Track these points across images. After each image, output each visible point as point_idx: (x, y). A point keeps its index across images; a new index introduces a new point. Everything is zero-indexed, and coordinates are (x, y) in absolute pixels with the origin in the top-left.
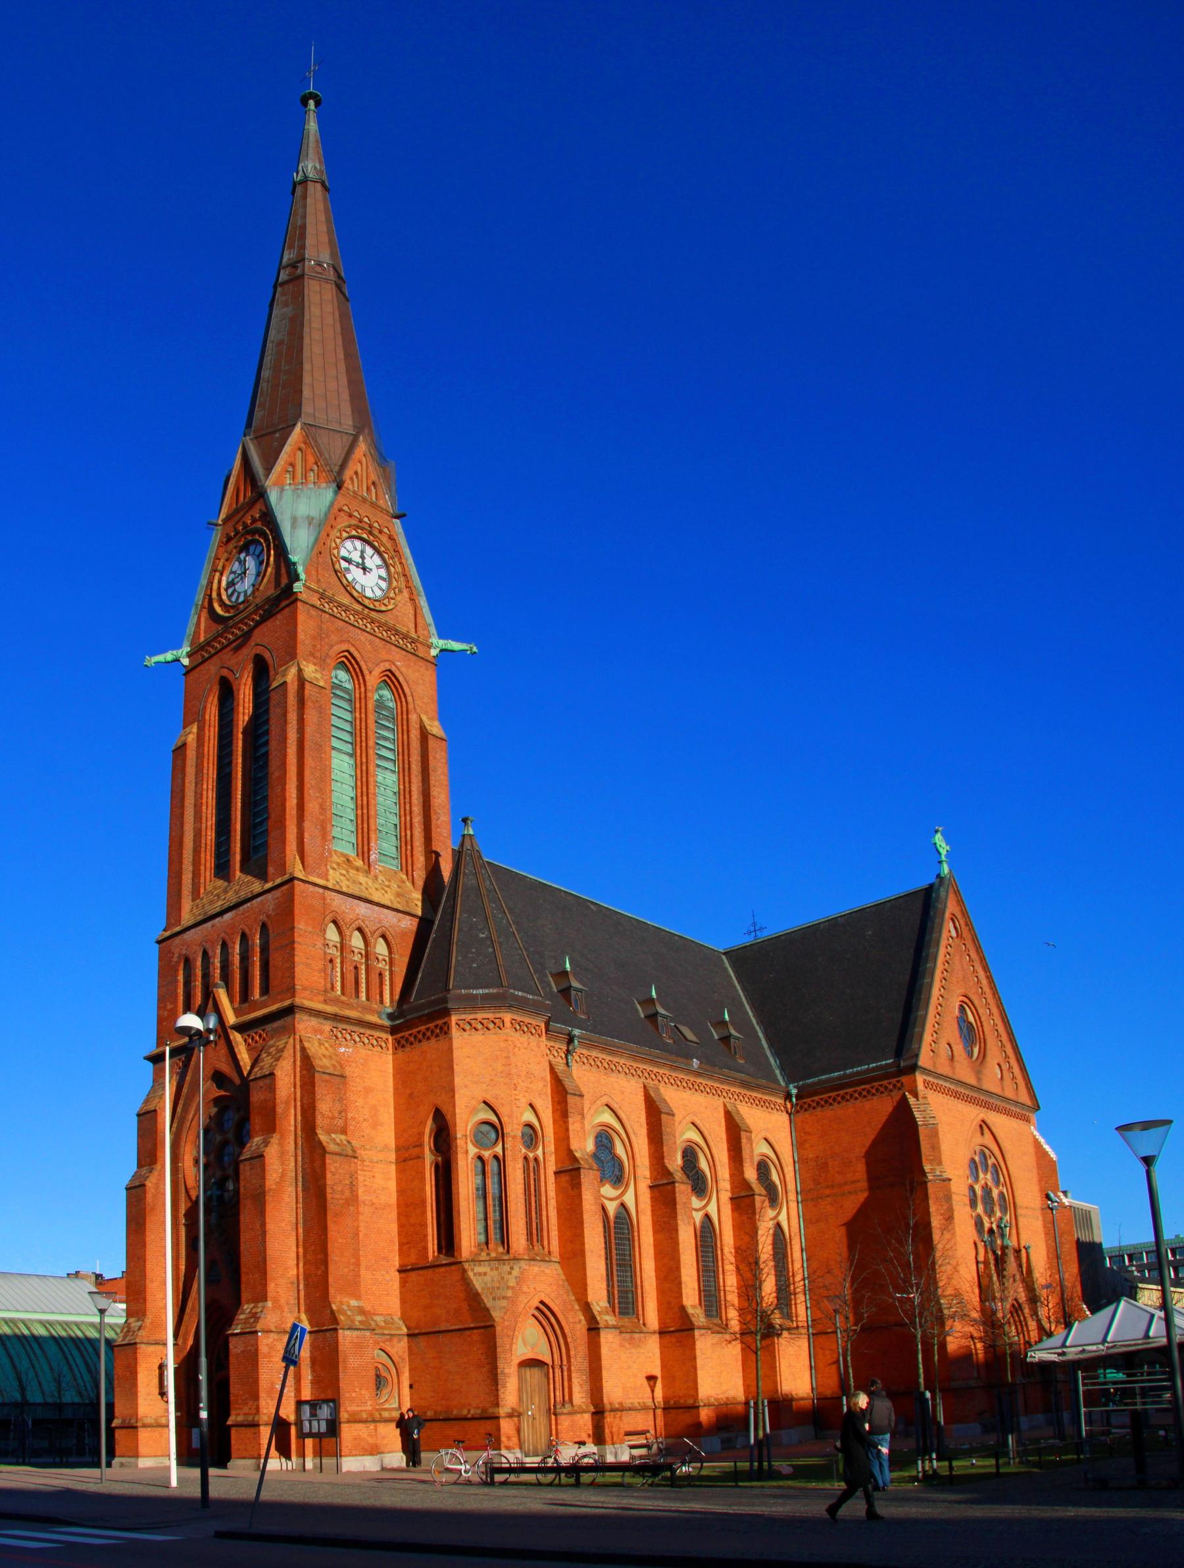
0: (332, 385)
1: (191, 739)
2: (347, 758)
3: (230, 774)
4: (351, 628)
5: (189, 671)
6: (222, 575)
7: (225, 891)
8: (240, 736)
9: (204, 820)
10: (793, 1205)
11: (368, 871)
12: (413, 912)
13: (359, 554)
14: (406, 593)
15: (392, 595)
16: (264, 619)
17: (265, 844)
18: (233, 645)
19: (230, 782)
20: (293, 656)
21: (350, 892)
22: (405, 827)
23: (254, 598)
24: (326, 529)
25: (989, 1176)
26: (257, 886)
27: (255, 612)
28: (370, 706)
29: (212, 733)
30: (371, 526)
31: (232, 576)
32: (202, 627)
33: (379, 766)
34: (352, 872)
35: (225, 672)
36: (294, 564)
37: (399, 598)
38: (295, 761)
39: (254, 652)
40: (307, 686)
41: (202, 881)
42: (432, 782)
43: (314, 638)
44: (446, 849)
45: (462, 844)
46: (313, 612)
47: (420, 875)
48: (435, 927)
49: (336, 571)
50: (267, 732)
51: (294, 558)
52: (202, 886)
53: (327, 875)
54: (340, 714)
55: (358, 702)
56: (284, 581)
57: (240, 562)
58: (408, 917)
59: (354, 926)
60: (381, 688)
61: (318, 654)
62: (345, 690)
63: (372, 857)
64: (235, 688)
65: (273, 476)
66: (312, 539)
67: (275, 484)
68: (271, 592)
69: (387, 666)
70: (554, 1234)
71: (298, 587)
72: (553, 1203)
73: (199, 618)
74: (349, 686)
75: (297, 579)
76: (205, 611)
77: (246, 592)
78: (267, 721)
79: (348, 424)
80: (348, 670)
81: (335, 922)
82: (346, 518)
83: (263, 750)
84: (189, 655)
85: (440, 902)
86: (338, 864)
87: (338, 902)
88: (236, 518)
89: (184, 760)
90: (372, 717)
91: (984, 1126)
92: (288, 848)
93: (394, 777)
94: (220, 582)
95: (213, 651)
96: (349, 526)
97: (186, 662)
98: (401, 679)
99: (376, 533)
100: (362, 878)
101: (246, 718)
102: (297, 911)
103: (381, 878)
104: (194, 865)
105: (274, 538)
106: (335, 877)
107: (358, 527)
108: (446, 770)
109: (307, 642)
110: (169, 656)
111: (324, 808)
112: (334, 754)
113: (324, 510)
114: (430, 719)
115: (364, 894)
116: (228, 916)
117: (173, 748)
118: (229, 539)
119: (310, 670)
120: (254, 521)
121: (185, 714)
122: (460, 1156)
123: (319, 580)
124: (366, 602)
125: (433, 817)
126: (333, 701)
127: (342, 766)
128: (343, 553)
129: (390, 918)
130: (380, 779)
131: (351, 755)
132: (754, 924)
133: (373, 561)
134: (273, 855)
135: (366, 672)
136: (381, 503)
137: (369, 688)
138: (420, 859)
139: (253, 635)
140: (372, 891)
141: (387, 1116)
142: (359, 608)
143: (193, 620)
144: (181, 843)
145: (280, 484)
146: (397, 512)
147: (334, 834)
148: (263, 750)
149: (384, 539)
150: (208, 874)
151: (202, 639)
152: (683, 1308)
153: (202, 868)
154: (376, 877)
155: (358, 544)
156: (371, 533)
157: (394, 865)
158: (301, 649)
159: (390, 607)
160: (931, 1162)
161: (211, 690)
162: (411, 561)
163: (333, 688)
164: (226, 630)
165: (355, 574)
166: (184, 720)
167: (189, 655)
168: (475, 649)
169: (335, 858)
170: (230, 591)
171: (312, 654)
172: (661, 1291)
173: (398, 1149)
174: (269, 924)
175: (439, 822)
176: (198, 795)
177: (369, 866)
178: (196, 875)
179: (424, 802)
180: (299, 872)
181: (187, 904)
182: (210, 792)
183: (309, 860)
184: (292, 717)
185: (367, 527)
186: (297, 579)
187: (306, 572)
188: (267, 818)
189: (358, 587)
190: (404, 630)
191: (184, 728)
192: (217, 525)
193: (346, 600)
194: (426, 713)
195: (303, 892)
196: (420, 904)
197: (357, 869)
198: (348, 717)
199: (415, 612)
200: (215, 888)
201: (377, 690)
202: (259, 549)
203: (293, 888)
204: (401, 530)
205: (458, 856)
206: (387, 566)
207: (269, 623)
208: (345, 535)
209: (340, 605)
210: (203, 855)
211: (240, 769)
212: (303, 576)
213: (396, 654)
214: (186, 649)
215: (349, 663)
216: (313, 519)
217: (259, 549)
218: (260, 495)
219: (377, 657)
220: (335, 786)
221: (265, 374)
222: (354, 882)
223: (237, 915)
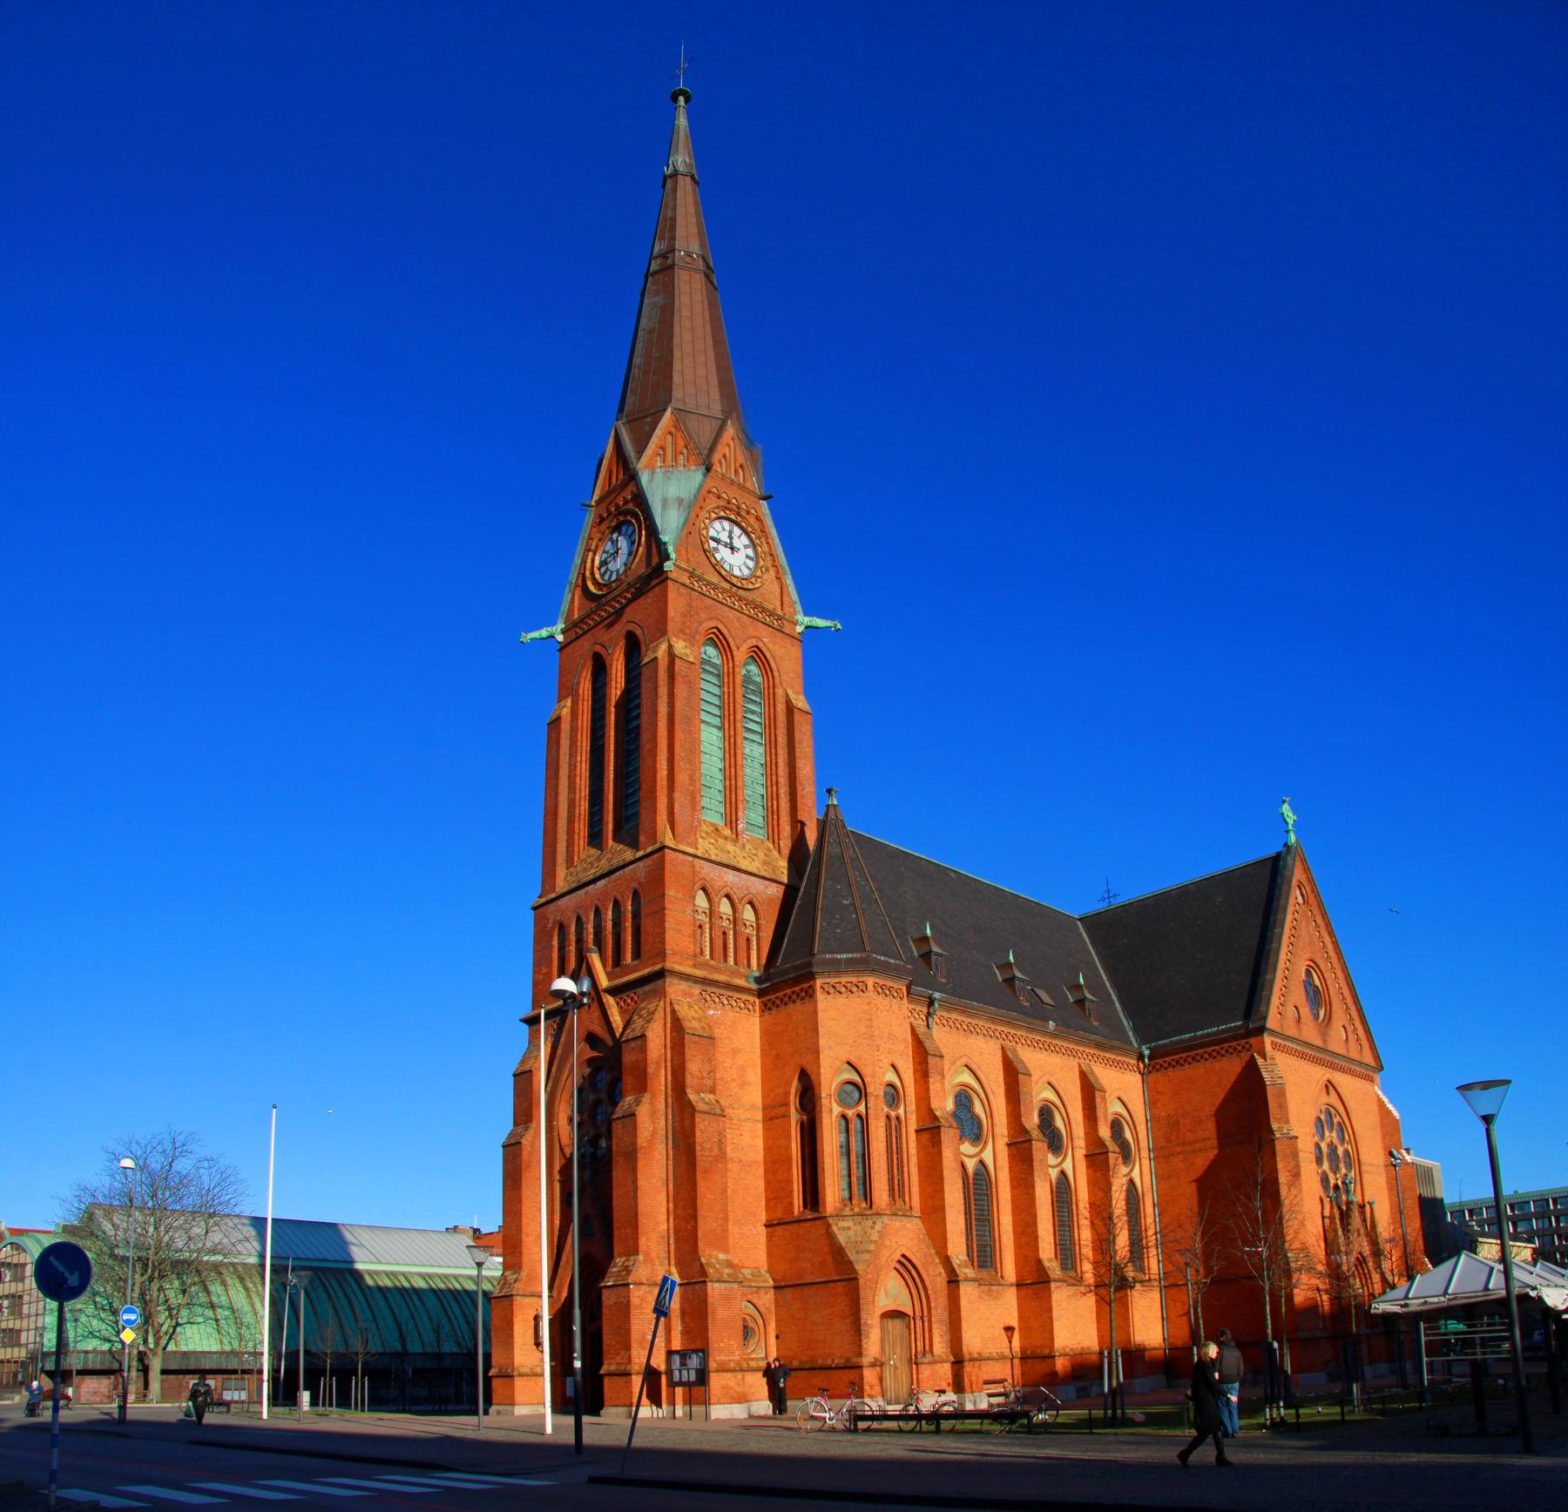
0: (701, 371)
1: (566, 712)
2: (715, 731)
5: (563, 647)
7: (599, 860)
10: (1146, 1162)
11: (736, 840)
14: (772, 572)
16: (635, 597)
17: (637, 815)
20: (664, 633)
22: (771, 798)
24: (695, 509)
25: (1334, 1134)
26: (629, 855)
27: (627, 591)
28: (738, 681)
34: (721, 841)
35: (598, 648)
40: (677, 661)
44: (811, 818)
45: (827, 815)
46: (683, 590)
47: (786, 844)
51: (664, 538)
54: (709, 689)
55: (726, 677)
56: (655, 560)
62: (714, 666)
66: (682, 520)
67: (647, 467)
68: (643, 571)
70: (915, 1190)
71: (668, 566)
72: (914, 1160)
74: (717, 661)
75: (668, 558)
78: (639, 696)
79: (717, 408)
80: (716, 646)
81: (704, 889)
83: (635, 723)
84: (564, 632)
87: (706, 870)
89: (559, 733)
90: (739, 692)
91: (1329, 1086)
93: (762, 750)
97: (560, 638)
100: (730, 847)
103: (748, 846)
106: (704, 846)
110: (544, 633)
111: (693, 779)
112: (703, 726)
118: (602, 520)
119: (680, 647)
120: (626, 502)
122: (825, 1115)
124: (734, 581)
125: (799, 788)
127: (710, 739)
128: (712, 533)
129: (757, 886)
130: (747, 751)
131: (719, 728)
132: (1108, 891)
133: (741, 541)
134: (645, 823)
138: (786, 829)
139: (625, 612)
140: (740, 859)
141: (755, 1076)
142: (727, 586)
143: (568, 597)
145: (651, 467)
149: (752, 520)
152: (1039, 1261)
154: (744, 846)
155: (726, 524)
156: (738, 514)
157: (760, 834)
158: (671, 627)
160: (1278, 1120)
162: (777, 541)
164: (599, 608)
165: (723, 553)
167: (564, 632)
169: (704, 827)
171: (682, 631)
172: (1018, 1245)
173: (765, 1108)
180: (669, 842)
181: (561, 872)
184: (663, 691)
186: (668, 558)
187: (677, 551)
190: (771, 607)
193: (715, 579)
197: (726, 838)
198: (717, 691)
199: (781, 590)
203: (663, 856)
205: (823, 825)
207: (641, 601)
209: (709, 583)
212: (673, 556)
213: (764, 632)
214: (561, 626)
215: (718, 639)
218: (632, 477)
220: (704, 758)
221: (637, 360)
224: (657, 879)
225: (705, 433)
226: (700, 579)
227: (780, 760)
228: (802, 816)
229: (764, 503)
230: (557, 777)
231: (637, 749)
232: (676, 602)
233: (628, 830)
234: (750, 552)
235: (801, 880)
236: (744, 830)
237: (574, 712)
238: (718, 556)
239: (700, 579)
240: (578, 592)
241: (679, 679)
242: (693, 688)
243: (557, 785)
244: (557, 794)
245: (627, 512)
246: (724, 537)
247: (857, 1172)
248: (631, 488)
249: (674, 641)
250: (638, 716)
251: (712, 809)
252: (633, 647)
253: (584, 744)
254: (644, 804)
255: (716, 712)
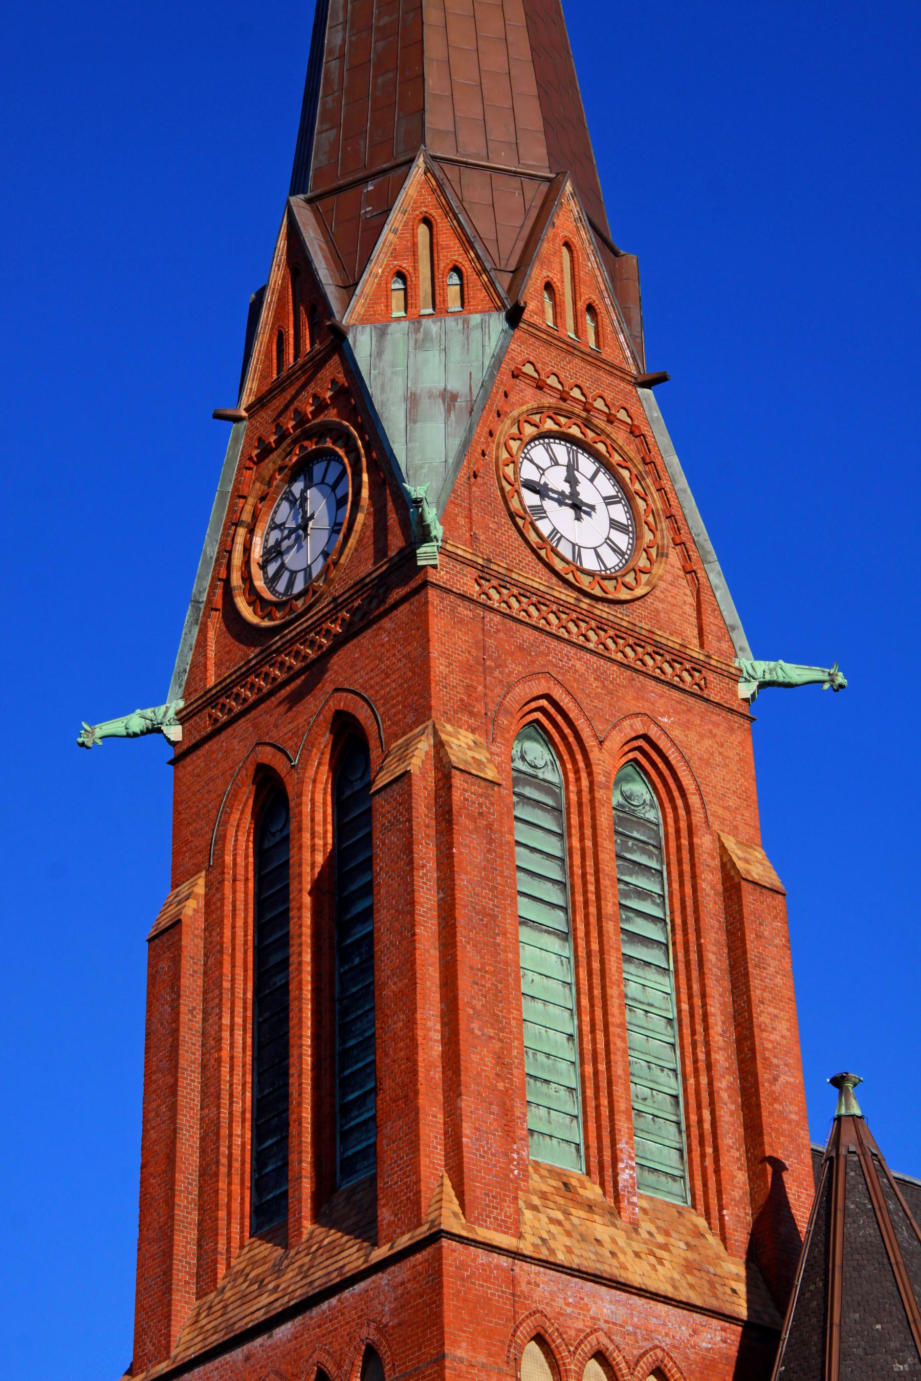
0: (494, 60)
1: (192, 908)
2: (554, 944)
3: (285, 989)
4: (554, 643)
5: (181, 755)
6: (251, 531)
7: (278, 1270)
8: (307, 900)
9: (225, 1101)
11: (616, 1211)
12: (727, 1309)
13: (562, 472)
14: (674, 557)
15: (643, 562)
16: (351, 633)
17: (370, 1153)
18: (284, 693)
19: (286, 1009)
20: (421, 711)
21: (575, 1262)
22: (696, 1103)
23: (329, 582)
24: (485, 416)
26: (353, 1256)
27: (331, 616)
28: (605, 820)
29: (240, 896)
30: (587, 408)
31: (275, 535)
32: (211, 654)
33: (629, 959)
34: (578, 1213)
35: (267, 755)
36: (418, 502)
37: (658, 570)
38: (435, 953)
39: (333, 705)
40: (458, 780)
41: (222, 1246)
42: (756, 994)
43: (468, 669)
44: (796, 1147)
45: (836, 1141)
46: (464, 611)
47: (739, 1218)
48: (783, 1347)
49: (512, 516)
50: (368, 889)
51: (416, 489)
52: (222, 1259)
53: (517, 1223)
54: (536, 842)
55: (575, 813)
56: (396, 542)
57: (292, 503)
58: (715, 1323)
59: (586, 1348)
60: (627, 779)
61: (479, 708)
62: (546, 786)
63: (624, 1176)
64: (290, 790)
65: (358, 305)
66: (455, 443)
67: (364, 320)
68: (367, 568)
69: (639, 726)
71: (427, 554)
73: (203, 632)
74: (553, 776)
75: (425, 536)
76: (216, 616)
77: (308, 570)
78: (368, 864)
79: (535, 157)
80: (549, 741)
81: (540, 1339)
82: (530, 392)
83: (360, 931)
84: (183, 718)
85: (790, 1285)
86: (543, 1196)
87: (544, 1287)
88: (279, 403)
89: (176, 961)
90: (608, 847)
92: (424, 1161)
93: (667, 984)
94: (247, 550)
95: (238, 708)
96: (539, 410)
97: (175, 732)
98: (673, 756)
99: (600, 422)
100: (601, 1229)
101: (320, 859)
102: (449, 1315)
103: (646, 1226)
104: (201, 1209)
105: (367, 446)
106: (537, 1228)
107: (559, 412)
108: (787, 964)
109: (453, 680)
110: (136, 722)
111: (507, 1060)
112: (525, 934)
113: (479, 377)
114: (745, 844)
115: (609, 1268)
116: (283, 1331)
117: (151, 932)
118: (266, 451)
119: (462, 744)
120: (321, 407)
121: (176, 853)
123: (474, 538)
124: (585, 582)
125: (764, 1076)
126: (518, 813)
127: (544, 961)
128: (528, 472)
129: (673, 1326)
130: (633, 989)
131: (563, 936)
133: (596, 488)
134: (389, 1178)
135: (590, 743)
136: (607, 353)
137: (600, 778)
138: (737, 1179)
139: (327, 667)
140: (628, 1259)
142: (568, 596)
143: (189, 635)
144: (171, 1159)
145: (381, 324)
146: (648, 372)
147: (532, 1123)
148: (360, 931)
149: (620, 436)
150: (236, 1228)
151: (212, 681)
153: (222, 1214)
154: (635, 1226)
155: (561, 450)
156: (587, 424)
157: (674, 1194)
158: (439, 697)
159: (639, 592)
161: (235, 794)
162: (682, 482)
163: (516, 782)
164: (267, 658)
165: (557, 519)
166: (174, 868)
167: (183, 718)
168: (840, 679)
169: (535, 1181)
170: (272, 568)
171: (465, 707)
174: (383, 1349)
175: (777, 1088)
176: (211, 1042)
177: (617, 1198)
178: (207, 1231)
179: (739, 1042)
180: (453, 1223)
181: (184, 1305)
182: (239, 1033)
183: (475, 1188)
184: (426, 852)
185: (578, 409)
186: (425, 536)
187: (444, 519)
188: (374, 1090)
189: (565, 550)
190: (674, 642)
191: (175, 885)
192: (238, 419)
193: (539, 580)
194: (734, 831)
195: (463, 1266)
196: (742, 1288)
197: (590, 1207)
198: (554, 847)
199: (695, 597)
200: (254, 1264)
201: (618, 782)
202: (334, 471)
203: (438, 1258)
204: (657, 414)
205: (828, 1167)
206: (627, 496)
207: (365, 639)
208: (529, 430)
209: (525, 592)
210: (222, 1185)
211: (307, 978)
212: (437, 530)
213: (659, 699)
214: (176, 704)
215: (551, 722)
216: (454, 397)
217: (334, 471)
218: (336, 342)
219: (614, 709)
220: (530, 1010)
221: (334, 38)
222: (583, 1238)
223: (306, 1328)
224: (425, 1315)
225: (504, 234)
226: (504, 583)
227: (714, 1008)
228: (775, 1146)
229: (647, 393)
230: (174, 1068)
231: (368, 992)
232: (449, 640)
233: (355, 1183)
234: (619, 513)
235: (782, 1311)
236: (636, 1184)
237: (212, 905)
238: (544, 527)
239: (504, 583)
240: (215, 623)
241: (462, 821)
242: (499, 847)
243: (173, 1089)
244: (173, 1109)
245: (325, 430)
246: (556, 480)
247: (536, 1262)
248: (333, 370)
249: (447, 731)
250: (368, 914)
251: (554, 1137)
252: (351, 749)
253: (240, 985)
254: (389, 1128)
255: (556, 897)
